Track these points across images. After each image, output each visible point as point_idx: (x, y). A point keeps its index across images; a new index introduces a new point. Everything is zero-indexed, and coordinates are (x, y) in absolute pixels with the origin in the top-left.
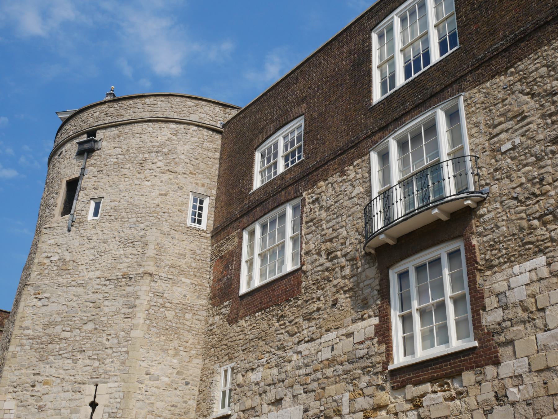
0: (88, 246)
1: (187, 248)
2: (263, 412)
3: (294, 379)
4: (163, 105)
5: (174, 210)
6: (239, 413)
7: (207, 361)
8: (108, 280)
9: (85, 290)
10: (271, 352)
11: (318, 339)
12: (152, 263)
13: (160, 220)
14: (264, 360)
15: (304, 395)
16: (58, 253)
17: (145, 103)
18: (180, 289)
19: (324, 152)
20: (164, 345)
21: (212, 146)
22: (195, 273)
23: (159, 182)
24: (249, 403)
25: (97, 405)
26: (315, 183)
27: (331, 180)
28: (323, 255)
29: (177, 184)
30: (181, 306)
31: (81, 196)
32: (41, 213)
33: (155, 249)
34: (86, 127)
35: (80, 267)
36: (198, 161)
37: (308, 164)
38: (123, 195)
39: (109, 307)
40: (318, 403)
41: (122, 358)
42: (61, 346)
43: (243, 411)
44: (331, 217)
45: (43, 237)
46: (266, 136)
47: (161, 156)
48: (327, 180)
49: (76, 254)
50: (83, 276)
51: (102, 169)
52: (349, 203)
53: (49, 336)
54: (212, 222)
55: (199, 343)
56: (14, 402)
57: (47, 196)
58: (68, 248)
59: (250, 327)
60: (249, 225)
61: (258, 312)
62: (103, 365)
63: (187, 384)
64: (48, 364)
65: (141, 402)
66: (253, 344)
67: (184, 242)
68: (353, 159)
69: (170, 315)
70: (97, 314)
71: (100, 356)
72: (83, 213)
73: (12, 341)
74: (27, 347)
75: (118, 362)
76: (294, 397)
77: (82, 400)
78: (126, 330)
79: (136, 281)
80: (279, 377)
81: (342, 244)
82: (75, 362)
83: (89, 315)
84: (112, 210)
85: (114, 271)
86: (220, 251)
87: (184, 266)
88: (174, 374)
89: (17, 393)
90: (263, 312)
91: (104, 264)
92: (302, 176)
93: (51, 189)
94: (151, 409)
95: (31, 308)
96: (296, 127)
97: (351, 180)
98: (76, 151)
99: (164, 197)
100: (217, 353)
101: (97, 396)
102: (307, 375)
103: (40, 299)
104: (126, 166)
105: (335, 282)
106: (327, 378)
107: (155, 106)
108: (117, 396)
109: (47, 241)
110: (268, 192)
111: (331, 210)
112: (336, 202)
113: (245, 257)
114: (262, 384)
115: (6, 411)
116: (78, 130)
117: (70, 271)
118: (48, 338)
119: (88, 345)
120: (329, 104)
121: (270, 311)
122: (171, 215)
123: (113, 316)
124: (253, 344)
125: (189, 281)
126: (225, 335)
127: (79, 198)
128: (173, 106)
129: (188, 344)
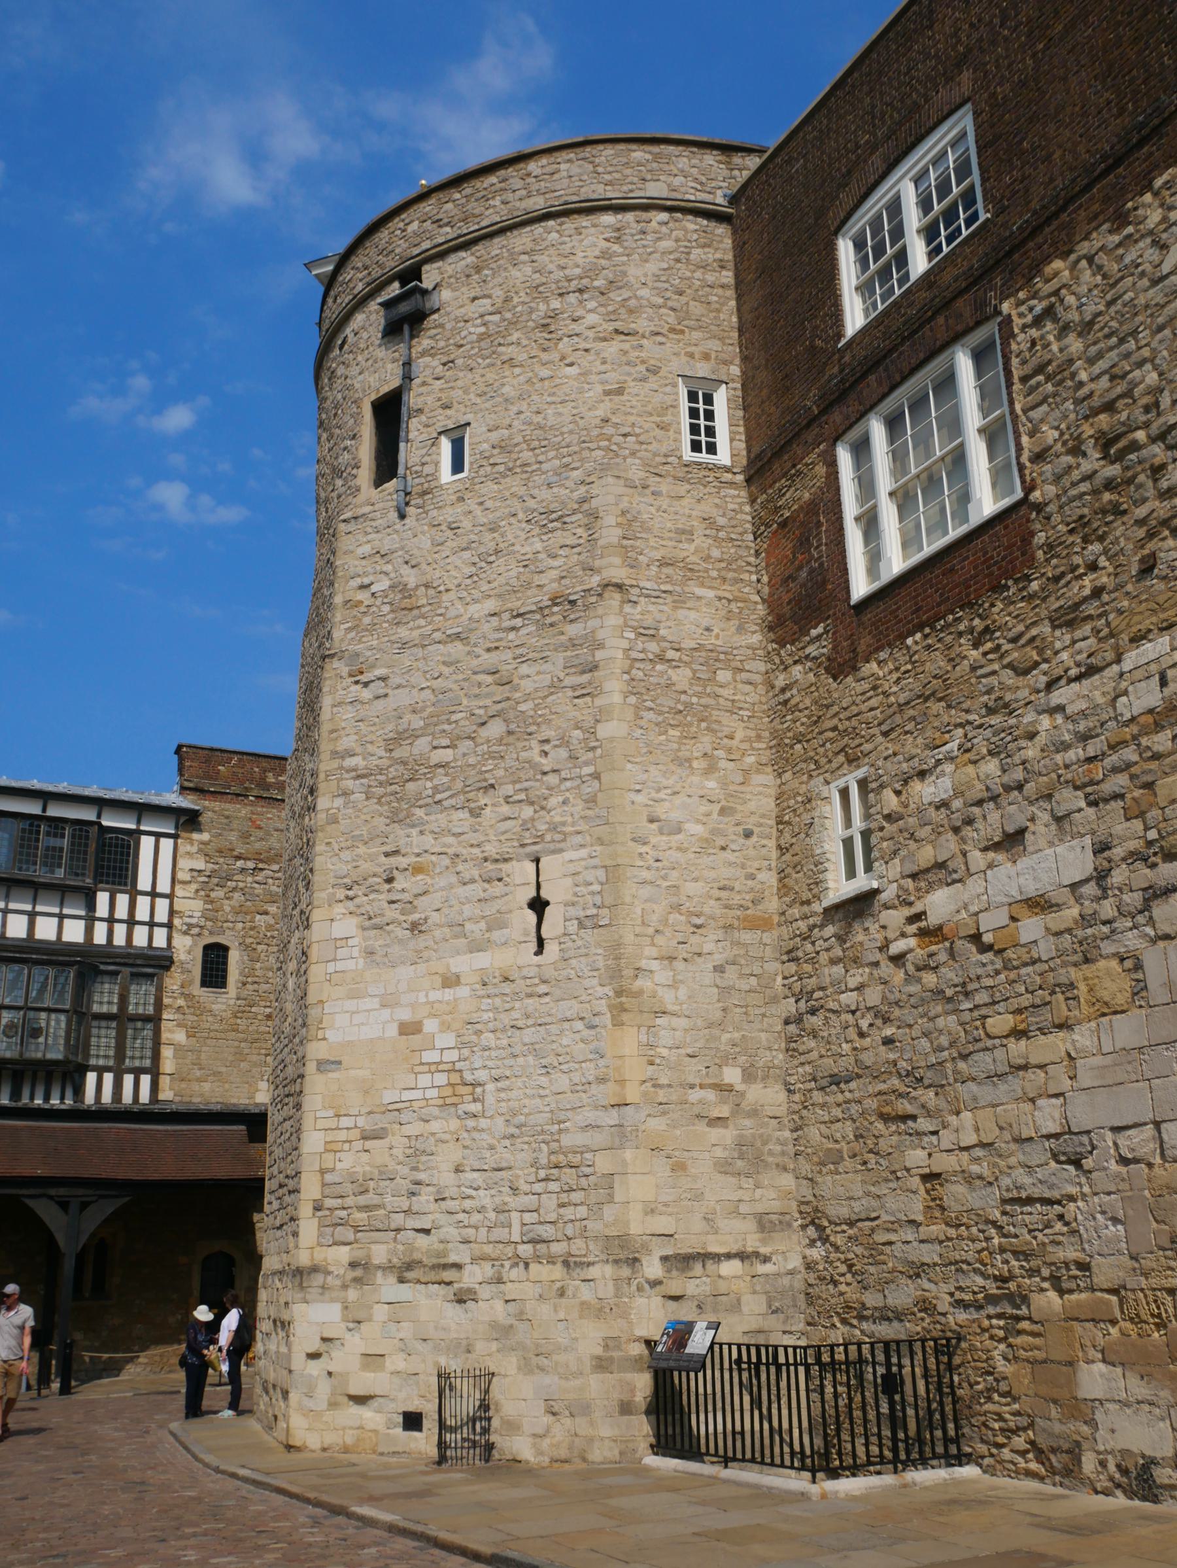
0: (454, 544)
1: (694, 513)
2: (972, 870)
3: (1054, 776)
4: (575, 169)
5: (646, 426)
6: (902, 882)
7: (788, 776)
8: (519, 615)
9: (468, 648)
10: (969, 722)
11: (1109, 665)
12: (617, 561)
13: (617, 456)
14: (954, 745)
15: (1091, 811)
16: (386, 574)
17: (529, 175)
18: (693, 615)
19: (1052, 180)
20: (679, 750)
21: (711, 256)
22: (723, 573)
23: (598, 363)
24: (926, 855)
25: (547, 903)
26: (1036, 268)
27: (1084, 248)
28: (1089, 452)
29: (643, 362)
30: (703, 654)
31: (415, 430)
32: (323, 495)
33: (619, 525)
34: (393, 264)
35: (445, 597)
36: (683, 299)
37: (1005, 225)
38: (515, 409)
39: (532, 678)
40: (1137, 825)
41: (587, 789)
42: (436, 782)
43: (914, 876)
44: (1101, 345)
45: (344, 543)
46: (863, 190)
47: (592, 298)
48: (1071, 252)
49: (429, 569)
50: (457, 617)
51: (452, 357)
52: (1155, 295)
53: (404, 763)
54: (744, 445)
55: (759, 737)
56: (354, 921)
57: (330, 450)
58: (407, 557)
59: (895, 676)
60: (851, 426)
61: (912, 634)
62: (543, 813)
63: (748, 834)
64: (413, 826)
65: (649, 887)
66: (912, 712)
67: (685, 502)
68: (1150, 172)
69: (681, 677)
70: (508, 699)
71: (533, 794)
72: (427, 469)
73: (322, 787)
74: (359, 797)
75: (579, 801)
76: (1058, 820)
77: (510, 897)
78: (586, 725)
79: (587, 607)
80: (1006, 779)
81: (1147, 409)
82: (476, 813)
83: (488, 702)
84: (496, 451)
85: (529, 593)
86: (777, 509)
87: (693, 559)
88: (715, 816)
89: (356, 901)
90: (927, 630)
91: (501, 580)
92: (991, 262)
93: (337, 431)
94: (675, 899)
95: (349, 708)
96: (952, 139)
97: (1151, 232)
98: (381, 328)
99: (617, 399)
100: (812, 754)
101: (543, 885)
102: (1090, 760)
103: (366, 684)
104: (510, 339)
105: (1141, 512)
106: (1156, 757)
107: (556, 176)
108: (590, 878)
109: (355, 550)
110: (894, 328)
111: (1096, 327)
112: (1110, 304)
113: (850, 507)
114: (957, 804)
115: (339, 943)
116: (374, 275)
117: (424, 610)
118: (401, 768)
119: (501, 773)
120: (1046, 48)
121: (948, 626)
122: (642, 438)
123: (546, 697)
124: (912, 712)
125: (711, 594)
126: (828, 707)
127: (411, 436)
128: (600, 169)
129: (735, 743)
